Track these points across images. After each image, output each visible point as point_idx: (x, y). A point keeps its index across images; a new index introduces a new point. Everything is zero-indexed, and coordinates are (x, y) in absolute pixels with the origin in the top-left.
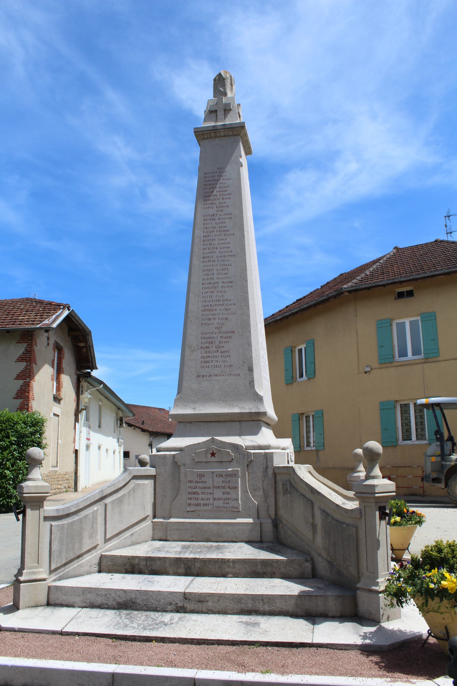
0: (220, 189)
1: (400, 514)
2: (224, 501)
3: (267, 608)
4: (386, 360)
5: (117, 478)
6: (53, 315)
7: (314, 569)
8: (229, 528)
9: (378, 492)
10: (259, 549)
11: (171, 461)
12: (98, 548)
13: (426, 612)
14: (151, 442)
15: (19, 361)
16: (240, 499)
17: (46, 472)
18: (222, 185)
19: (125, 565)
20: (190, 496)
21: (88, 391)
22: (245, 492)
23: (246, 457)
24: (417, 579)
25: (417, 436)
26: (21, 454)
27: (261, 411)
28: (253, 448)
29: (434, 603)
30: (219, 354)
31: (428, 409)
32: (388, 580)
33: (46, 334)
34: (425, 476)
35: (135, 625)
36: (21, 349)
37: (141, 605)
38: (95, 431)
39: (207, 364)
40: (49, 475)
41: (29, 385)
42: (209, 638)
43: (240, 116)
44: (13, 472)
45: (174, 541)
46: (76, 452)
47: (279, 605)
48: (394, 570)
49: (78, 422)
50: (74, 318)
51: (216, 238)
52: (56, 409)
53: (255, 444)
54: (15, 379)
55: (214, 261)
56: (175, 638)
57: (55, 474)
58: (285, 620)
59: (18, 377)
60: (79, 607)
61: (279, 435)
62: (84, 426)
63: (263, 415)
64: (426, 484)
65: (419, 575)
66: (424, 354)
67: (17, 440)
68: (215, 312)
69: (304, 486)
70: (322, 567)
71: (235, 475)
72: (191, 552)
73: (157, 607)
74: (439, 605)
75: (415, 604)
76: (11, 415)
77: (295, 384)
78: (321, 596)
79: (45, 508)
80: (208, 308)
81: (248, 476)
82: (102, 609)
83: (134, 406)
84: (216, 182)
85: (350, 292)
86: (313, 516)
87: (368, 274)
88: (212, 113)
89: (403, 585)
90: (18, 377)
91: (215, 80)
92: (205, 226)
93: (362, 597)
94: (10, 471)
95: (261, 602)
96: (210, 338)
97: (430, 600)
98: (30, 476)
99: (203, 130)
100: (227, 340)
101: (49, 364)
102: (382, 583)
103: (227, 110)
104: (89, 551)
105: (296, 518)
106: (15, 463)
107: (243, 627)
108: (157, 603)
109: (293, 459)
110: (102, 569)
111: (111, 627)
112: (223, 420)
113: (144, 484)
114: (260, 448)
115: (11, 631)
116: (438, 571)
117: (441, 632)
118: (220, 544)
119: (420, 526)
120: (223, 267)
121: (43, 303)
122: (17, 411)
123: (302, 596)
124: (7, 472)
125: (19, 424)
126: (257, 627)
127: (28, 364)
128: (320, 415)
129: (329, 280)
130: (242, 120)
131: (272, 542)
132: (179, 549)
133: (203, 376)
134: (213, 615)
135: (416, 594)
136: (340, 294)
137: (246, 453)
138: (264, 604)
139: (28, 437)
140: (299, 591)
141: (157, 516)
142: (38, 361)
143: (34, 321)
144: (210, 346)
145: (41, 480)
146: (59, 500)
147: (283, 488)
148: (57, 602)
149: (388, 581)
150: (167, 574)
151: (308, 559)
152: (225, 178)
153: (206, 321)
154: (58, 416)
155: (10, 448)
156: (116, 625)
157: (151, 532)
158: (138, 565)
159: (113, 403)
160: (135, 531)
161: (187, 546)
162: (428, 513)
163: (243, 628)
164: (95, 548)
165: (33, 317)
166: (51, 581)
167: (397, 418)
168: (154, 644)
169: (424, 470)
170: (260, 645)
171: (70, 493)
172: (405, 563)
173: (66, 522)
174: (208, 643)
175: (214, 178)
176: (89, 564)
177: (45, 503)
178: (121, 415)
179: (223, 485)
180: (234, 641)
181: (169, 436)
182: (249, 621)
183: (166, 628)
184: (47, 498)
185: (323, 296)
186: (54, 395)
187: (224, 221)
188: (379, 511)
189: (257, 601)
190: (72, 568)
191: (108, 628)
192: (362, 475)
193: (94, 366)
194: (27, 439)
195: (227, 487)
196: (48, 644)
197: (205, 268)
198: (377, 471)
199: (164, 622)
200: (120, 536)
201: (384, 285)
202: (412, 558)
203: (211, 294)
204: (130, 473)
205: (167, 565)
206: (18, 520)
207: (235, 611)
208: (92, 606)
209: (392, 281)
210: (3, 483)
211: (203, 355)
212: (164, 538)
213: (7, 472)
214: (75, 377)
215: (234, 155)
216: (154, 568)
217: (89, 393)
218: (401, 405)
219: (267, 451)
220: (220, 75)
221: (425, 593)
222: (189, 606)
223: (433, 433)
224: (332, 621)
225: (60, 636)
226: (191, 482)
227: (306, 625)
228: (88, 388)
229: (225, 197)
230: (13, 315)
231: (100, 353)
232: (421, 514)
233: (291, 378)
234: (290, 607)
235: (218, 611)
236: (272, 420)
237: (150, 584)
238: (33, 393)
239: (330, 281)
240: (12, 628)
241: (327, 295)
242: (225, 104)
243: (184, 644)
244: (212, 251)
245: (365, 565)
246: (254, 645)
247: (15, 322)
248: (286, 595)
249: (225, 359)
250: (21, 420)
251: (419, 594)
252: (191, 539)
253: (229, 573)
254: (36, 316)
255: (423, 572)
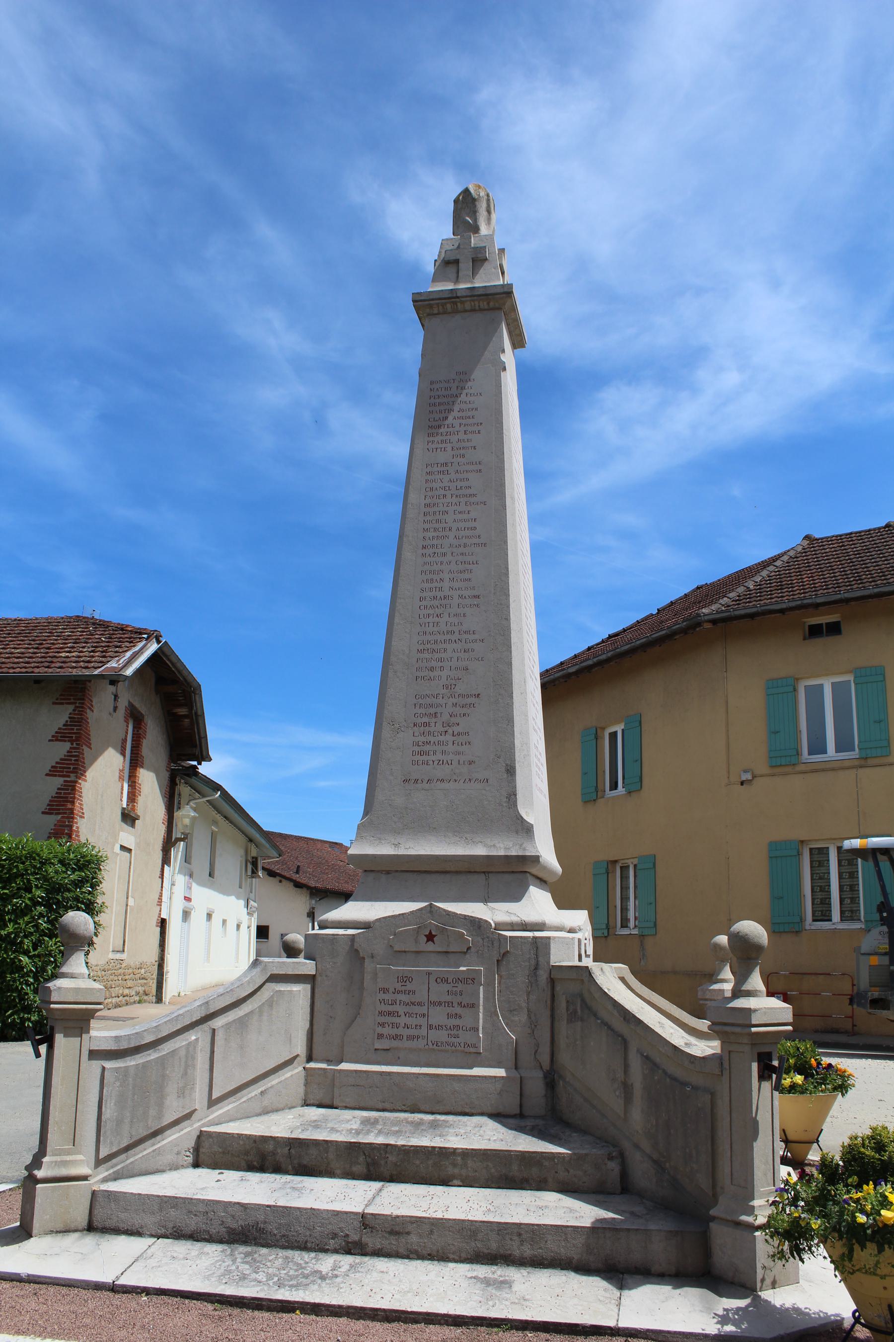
0: (460, 414)
1: (803, 1069)
2: (450, 1032)
3: (528, 1251)
4: (784, 759)
5: (239, 979)
6: (126, 651)
7: (624, 1175)
8: (457, 1086)
9: (757, 1023)
10: (516, 1130)
11: (347, 948)
12: (194, 1117)
13: (849, 1272)
14: (313, 908)
15: (57, 740)
16: (481, 1028)
17: (102, 962)
18: (464, 406)
19: (247, 1153)
20: (382, 1019)
21: (191, 803)
22: (491, 1014)
23: (496, 944)
24: (831, 1203)
25: (842, 912)
26: (53, 925)
27: (528, 854)
28: (510, 928)
29: (866, 1255)
30: (449, 738)
31: (865, 859)
32: (774, 1203)
33: (112, 689)
34: (858, 993)
35: (261, 1276)
36: (61, 716)
37: (275, 1235)
38: (201, 884)
39: (425, 758)
40: (107, 967)
41: (74, 789)
42: (409, 1310)
43: (503, 273)
44: (36, 960)
45: (346, 1108)
46: (163, 923)
47: (553, 1247)
48: (787, 1182)
49: (169, 866)
50: (169, 660)
51: (451, 509)
52: (127, 836)
53: (514, 919)
54: (47, 775)
55: (444, 555)
56: (340, 1307)
57: (118, 966)
58: (564, 1277)
59: (54, 772)
60: (152, 1236)
61: (561, 904)
62: (180, 872)
63: (533, 862)
64: (859, 1011)
65: (835, 1195)
66: (860, 749)
67: (47, 896)
68: (443, 655)
69: (610, 1007)
70: (642, 1171)
71: (473, 980)
72: (380, 1132)
73: (306, 1242)
74: (876, 1259)
75: (827, 1256)
76: (37, 845)
77: (601, 801)
78: (637, 1230)
79: (93, 1033)
80: (429, 646)
81: (499, 983)
82: (197, 1241)
83: (280, 835)
84: (453, 399)
85: (714, 622)
86: (626, 1067)
87: (752, 587)
88: (449, 264)
89: (803, 1216)
90: (54, 772)
91: (456, 201)
92: (430, 485)
93: (720, 1235)
94: (30, 957)
95: (515, 1238)
96: (431, 706)
97: (857, 1247)
98: (64, 969)
99: (431, 297)
100: (464, 711)
101: (115, 748)
102: (762, 1210)
103: (479, 259)
104: (176, 1123)
105: (592, 1071)
106: (40, 941)
107: (477, 1290)
108: (308, 1233)
109: (590, 951)
110: (200, 1160)
111: (213, 1279)
112: (453, 869)
113: (291, 991)
114: (525, 927)
115: (12, 1280)
116: (875, 1188)
117: (879, 1316)
118: (439, 1117)
119: (843, 1095)
120: (461, 567)
121: (108, 626)
122: (49, 838)
123: (598, 1229)
124: (24, 959)
125: (52, 864)
126: (507, 1290)
127: (75, 745)
128: (648, 866)
129: (673, 599)
130: (508, 280)
131: (542, 1117)
132: (355, 1125)
133: (416, 781)
134: (419, 1262)
135: (830, 1234)
136: (693, 626)
137: (496, 937)
138: (522, 1242)
139: (69, 890)
140: (593, 1220)
141: (314, 1056)
142: (94, 741)
143: (89, 662)
144: (432, 722)
145: (87, 976)
146: (124, 1019)
147: (567, 1009)
148: (108, 1224)
149: (773, 1207)
150: (330, 1174)
151: (614, 1154)
152: (471, 391)
153: (426, 673)
154: (129, 850)
155: (32, 911)
156: (223, 1275)
157: (301, 1090)
158: (274, 1154)
159: (239, 829)
160: (269, 1085)
161: (372, 1120)
162: (861, 1069)
163: (477, 1292)
164: (188, 1116)
165: (87, 654)
166: (97, 1183)
167: (798, 876)
168: (298, 1316)
169: (855, 983)
170: (511, 1328)
171: (147, 1004)
172: (808, 1170)
173: (133, 1063)
174: (406, 1318)
175: (449, 392)
176: (176, 1150)
177: (93, 1023)
178: (254, 852)
179: (449, 998)
180: (459, 1316)
181: (346, 897)
182: (491, 1276)
183: (324, 1284)
184: (98, 1014)
185: (662, 630)
186: (124, 809)
187: (465, 475)
188: (759, 1062)
189: (507, 1237)
190: (140, 1155)
191: (207, 1282)
192: (728, 987)
193: (204, 753)
194: (67, 894)
195: (455, 1004)
196: (85, 1309)
197: (427, 567)
198: (756, 981)
199: (321, 1272)
200: (239, 1095)
201: (782, 611)
202: (823, 1159)
203: (436, 619)
204: (264, 969)
205: (331, 1156)
206: (38, 1055)
207: (464, 1255)
208: (178, 1234)
209: (799, 602)
210: (14, 981)
211: (417, 739)
212: (327, 1101)
213: (24, 959)
214: (166, 775)
215: (491, 347)
216: (305, 1163)
217: (192, 807)
218: (811, 849)
219: (538, 934)
220: (466, 192)
221: (847, 1232)
222: (371, 1241)
223: (875, 909)
224: (659, 1284)
225: (111, 1294)
226: (385, 990)
227: (605, 1290)
228: (192, 798)
229: (470, 429)
230: (49, 648)
231: (215, 732)
232: (845, 1071)
233: (593, 789)
234: (574, 1250)
235: (429, 1255)
236: (551, 872)
237: (296, 1194)
238: (81, 804)
239: (677, 600)
240: (16, 1274)
241: (668, 628)
242: (475, 248)
243: (358, 1319)
244: (441, 534)
245: (727, 1170)
246: (498, 1326)
247: (52, 662)
248: (568, 1226)
249: (460, 749)
250: (55, 857)
251: (836, 1235)
252: (380, 1106)
253: (453, 1177)
254: (93, 651)
255: (845, 1189)
